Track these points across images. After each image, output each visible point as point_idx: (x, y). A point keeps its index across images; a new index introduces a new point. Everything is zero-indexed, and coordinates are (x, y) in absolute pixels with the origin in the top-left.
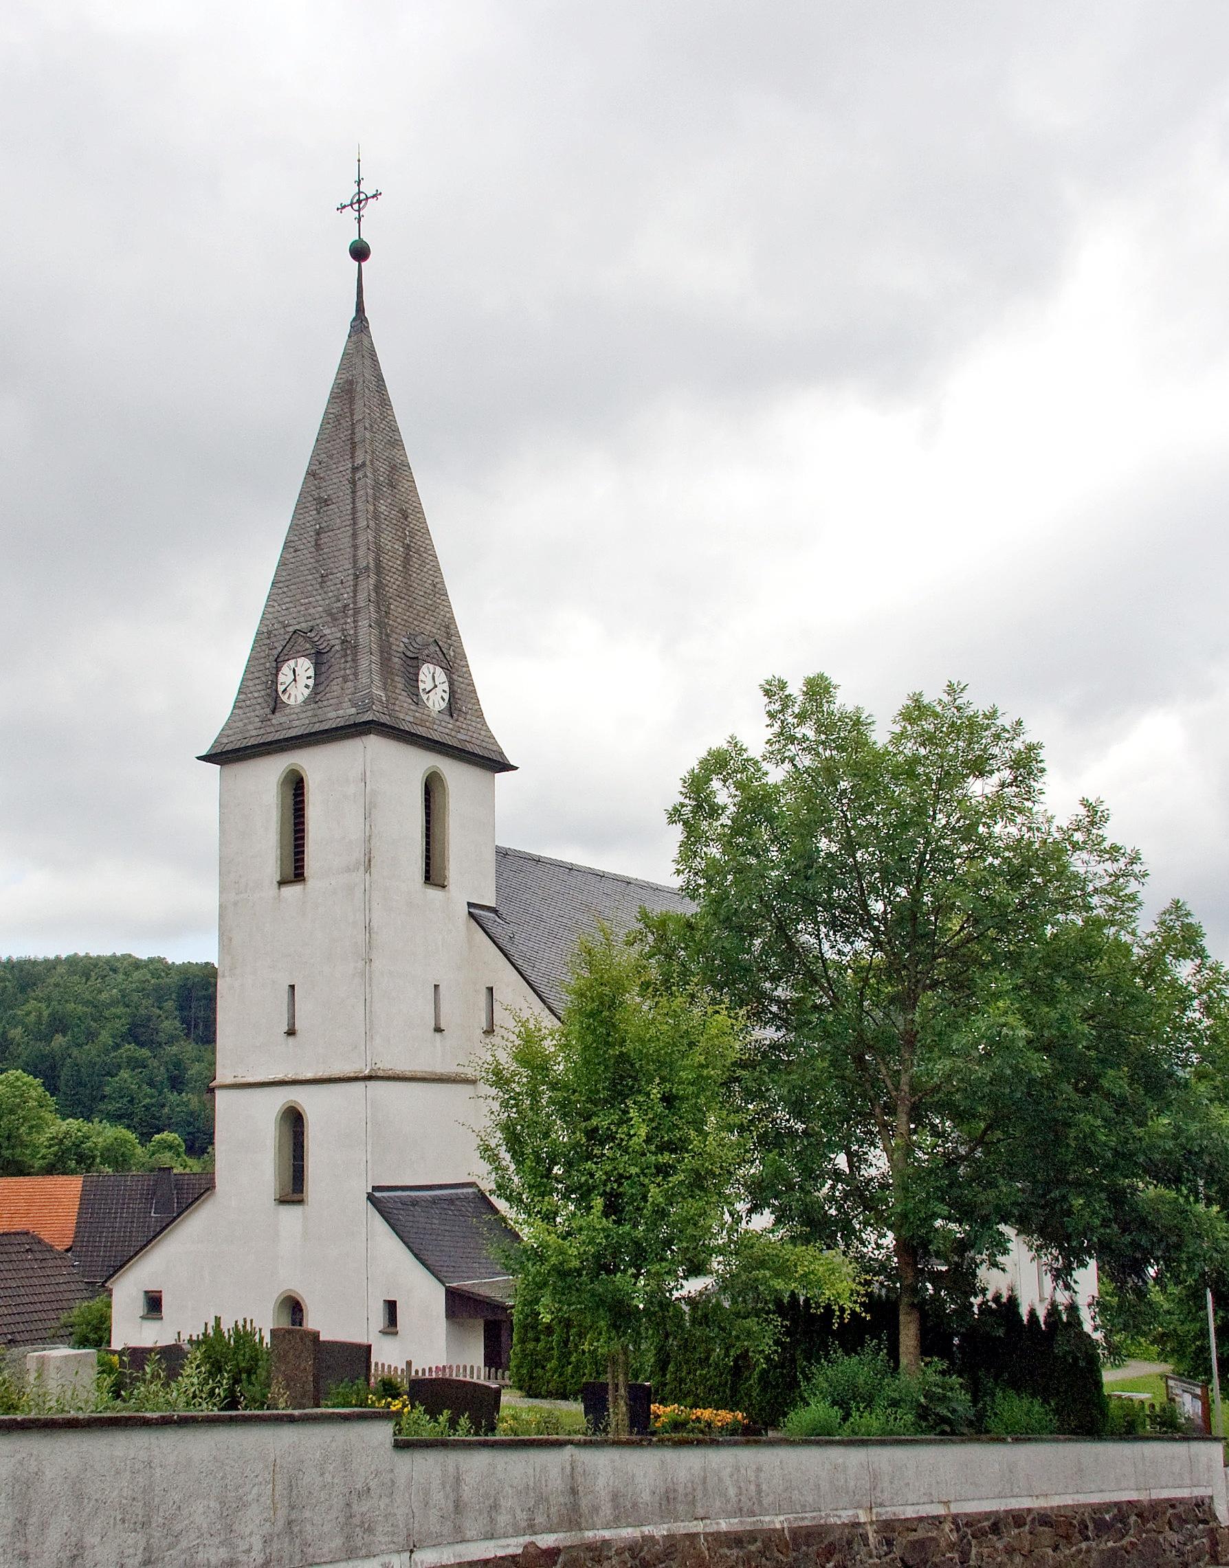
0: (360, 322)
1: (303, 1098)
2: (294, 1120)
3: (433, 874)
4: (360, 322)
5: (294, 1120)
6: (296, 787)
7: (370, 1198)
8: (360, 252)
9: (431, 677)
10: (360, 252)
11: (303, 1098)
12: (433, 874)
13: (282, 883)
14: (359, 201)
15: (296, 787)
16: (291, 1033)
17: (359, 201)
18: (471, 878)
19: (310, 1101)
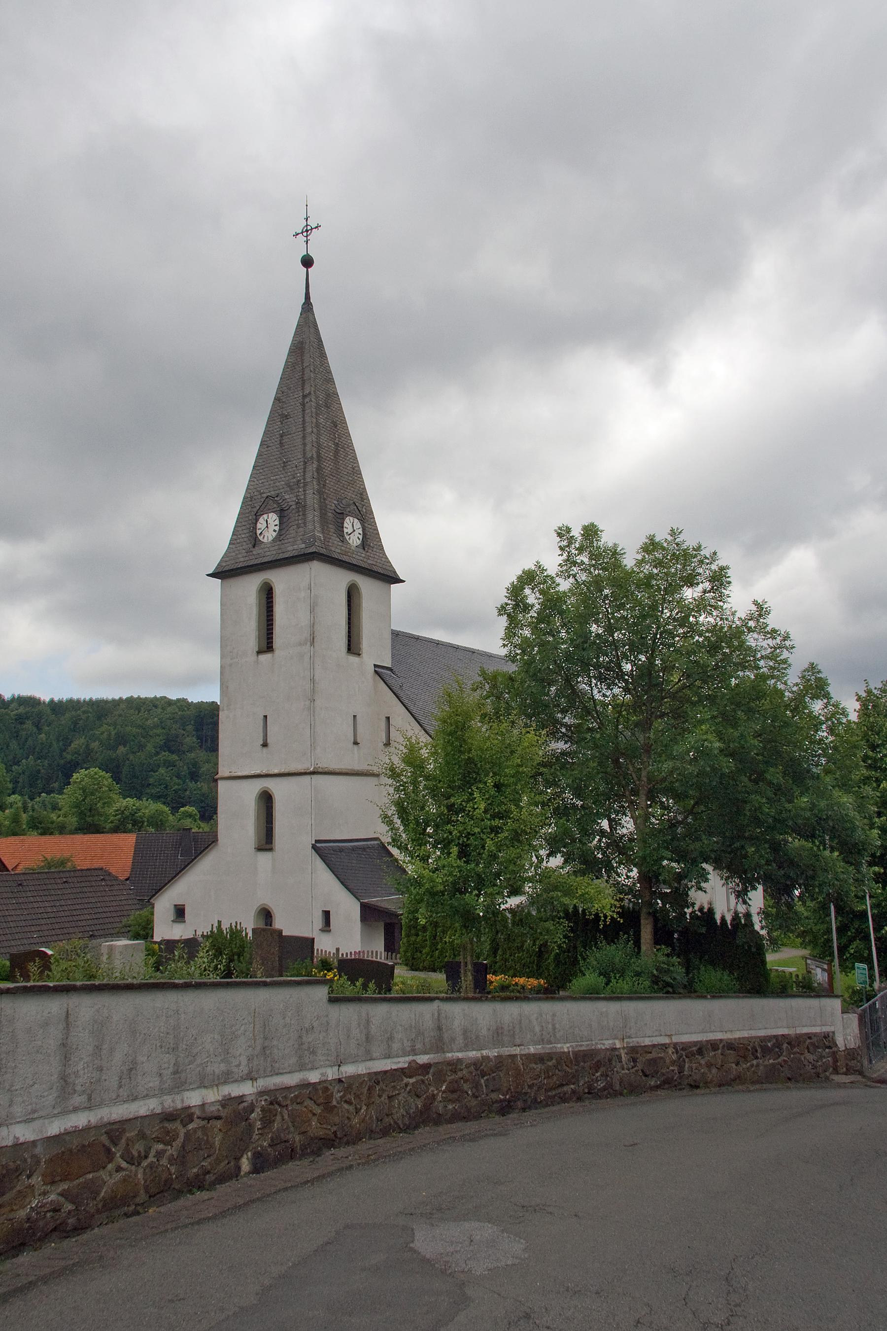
0: (307, 306)
1: (272, 785)
2: (266, 800)
3: (353, 647)
4: (307, 306)
5: (266, 800)
6: (268, 593)
7: (314, 847)
8: (307, 262)
9: (352, 526)
10: (307, 262)
11: (272, 785)
12: (353, 647)
13: (259, 652)
14: (307, 231)
15: (268, 593)
16: (265, 745)
17: (307, 231)
18: (376, 650)
19: (277, 788)
